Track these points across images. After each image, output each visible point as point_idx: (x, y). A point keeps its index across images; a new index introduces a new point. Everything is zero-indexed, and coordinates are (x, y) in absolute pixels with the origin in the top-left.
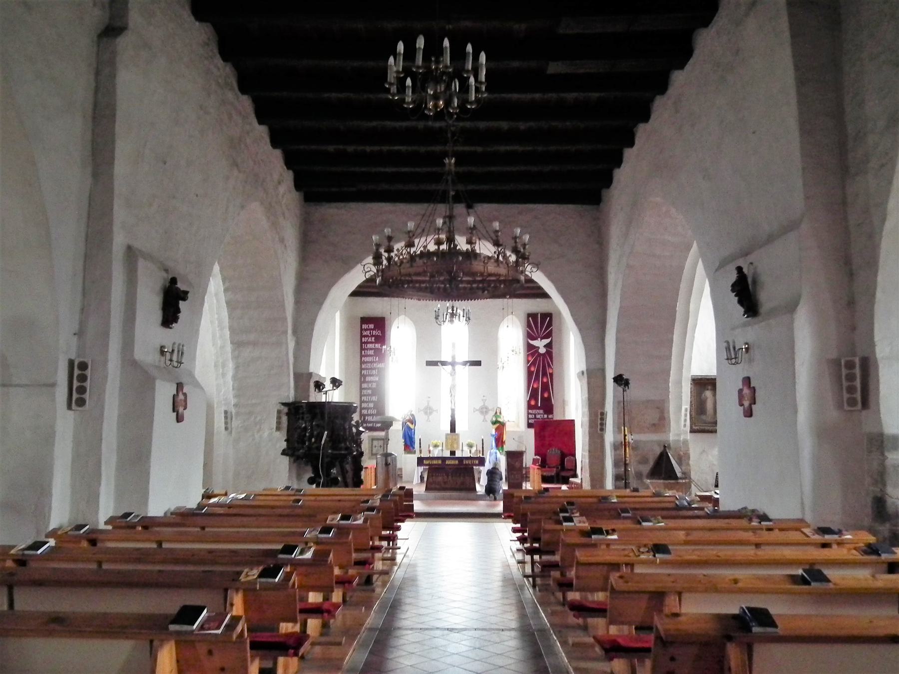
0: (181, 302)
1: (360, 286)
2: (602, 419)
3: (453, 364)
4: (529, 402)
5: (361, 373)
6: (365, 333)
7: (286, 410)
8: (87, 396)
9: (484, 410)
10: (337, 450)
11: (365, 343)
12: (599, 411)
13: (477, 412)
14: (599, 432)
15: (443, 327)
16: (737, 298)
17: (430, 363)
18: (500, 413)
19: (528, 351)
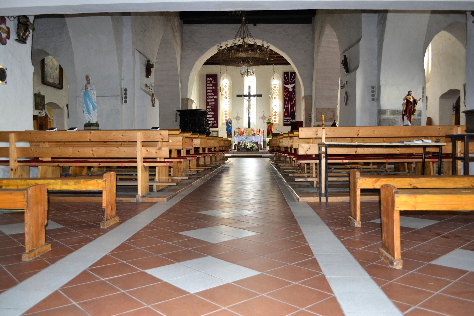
0: (151, 69)
1: (208, 60)
2: (310, 117)
3: (249, 96)
4: (284, 114)
5: (206, 101)
6: (208, 82)
7: (179, 113)
8: (127, 100)
9: (263, 118)
10: (201, 129)
11: (208, 87)
12: (309, 114)
13: (261, 119)
14: (309, 122)
15: (244, 77)
16: (343, 66)
17: (238, 96)
18: (271, 119)
19: (284, 90)
